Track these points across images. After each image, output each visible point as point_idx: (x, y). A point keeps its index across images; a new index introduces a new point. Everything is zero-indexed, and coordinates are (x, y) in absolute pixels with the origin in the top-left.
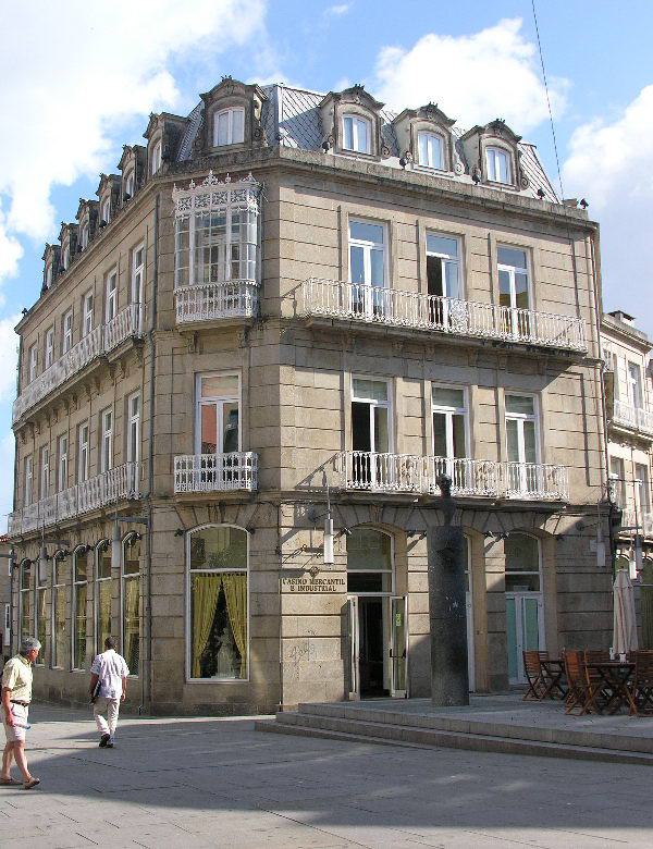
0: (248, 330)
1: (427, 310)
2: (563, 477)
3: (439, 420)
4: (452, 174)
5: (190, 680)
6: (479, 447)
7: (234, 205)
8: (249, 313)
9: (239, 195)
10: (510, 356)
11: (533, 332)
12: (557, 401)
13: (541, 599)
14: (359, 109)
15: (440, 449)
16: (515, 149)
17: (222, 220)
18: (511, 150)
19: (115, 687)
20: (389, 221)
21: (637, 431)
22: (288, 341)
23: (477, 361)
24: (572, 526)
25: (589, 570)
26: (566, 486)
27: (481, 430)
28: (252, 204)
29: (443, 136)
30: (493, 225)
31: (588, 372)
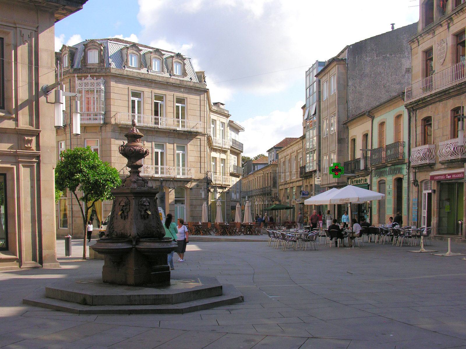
0: (101, 127)
1: (153, 120)
2: (193, 171)
3: (157, 153)
4: (163, 73)
5: (60, 228)
6: (168, 162)
7: (98, 87)
8: (102, 122)
9: (98, 84)
10: (178, 134)
11: (186, 126)
12: (192, 147)
13: (185, 207)
14: (134, 52)
15: (157, 163)
16: (184, 62)
17: (94, 91)
18: (182, 63)
19: (308, 214)
20: (143, 92)
21: (222, 148)
22: (114, 131)
23: (169, 135)
24: (195, 185)
25: (200, 199)
26: (194, 174)
27: (169, 157)
28: (103, 87)
29: (161, 60)
30: (175, 91)
31: (202, 138)
